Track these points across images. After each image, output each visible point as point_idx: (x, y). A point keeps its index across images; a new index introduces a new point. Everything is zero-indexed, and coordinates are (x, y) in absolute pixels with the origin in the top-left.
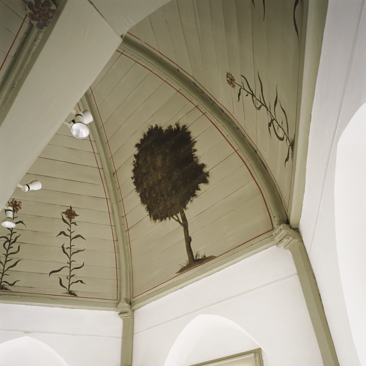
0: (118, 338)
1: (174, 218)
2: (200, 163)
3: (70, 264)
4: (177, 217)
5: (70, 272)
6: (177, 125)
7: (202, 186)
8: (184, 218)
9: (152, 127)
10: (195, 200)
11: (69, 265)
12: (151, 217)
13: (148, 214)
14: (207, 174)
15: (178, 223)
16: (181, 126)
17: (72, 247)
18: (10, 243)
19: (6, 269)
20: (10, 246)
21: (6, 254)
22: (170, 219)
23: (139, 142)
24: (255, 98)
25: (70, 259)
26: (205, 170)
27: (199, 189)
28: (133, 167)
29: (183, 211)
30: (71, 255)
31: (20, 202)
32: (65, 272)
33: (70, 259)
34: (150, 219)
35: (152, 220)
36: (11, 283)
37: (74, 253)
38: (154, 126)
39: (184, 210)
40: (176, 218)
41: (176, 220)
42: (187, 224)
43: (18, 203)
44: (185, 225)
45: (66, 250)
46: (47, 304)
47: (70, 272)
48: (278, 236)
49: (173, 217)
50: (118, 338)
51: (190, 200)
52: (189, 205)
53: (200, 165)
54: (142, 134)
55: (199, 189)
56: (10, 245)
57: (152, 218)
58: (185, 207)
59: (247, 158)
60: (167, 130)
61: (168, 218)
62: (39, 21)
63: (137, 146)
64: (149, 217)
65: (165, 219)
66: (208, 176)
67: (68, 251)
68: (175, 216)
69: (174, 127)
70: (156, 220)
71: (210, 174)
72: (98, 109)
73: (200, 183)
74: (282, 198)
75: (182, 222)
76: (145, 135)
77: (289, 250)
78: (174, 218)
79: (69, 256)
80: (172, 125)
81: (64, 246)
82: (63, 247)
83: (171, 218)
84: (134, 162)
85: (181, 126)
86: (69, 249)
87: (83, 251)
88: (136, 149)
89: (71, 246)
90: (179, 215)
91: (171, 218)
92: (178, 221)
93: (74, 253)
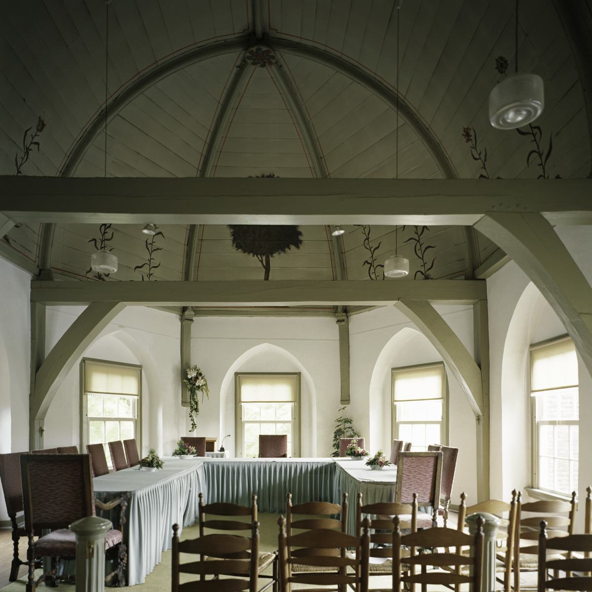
1: (258, 258)
2: (299, 230)
4: (262, 259)
5: (150, 269)
7: (292, 247)
8: (268, 262)
10: (282, 254)
11: (148, 262)
12: (233, 243)
13: (232, 238)
14: (301, 242)
15: (261, 263)
18: (105, 227)
20: (106, 231)
22: (254, 256)
24: (203, 501)
26: (301, 238)
27: (290, 249)
30: (152, 252)
32: (146, 269)
35: (235, 246)
37: (154, 250)
39: (270, 257)
40: (260, 259)
41: (260, 260)
42: (269, 269)
46: (359, 312)
47: (150, 269)
48: (23, 498)
52: (276, 255)
55: (290, 249)
57: (235, 245)
58: (272, 254)
61: (251, 254)
64: (231, 242)
65: (249, 253)
66: (301, 243)
67: (149, 247)
68: (259, 256)
70: (239, 248)
71: (303, 243)
72: (237, 108)
73: (292, 244)
74: (345, 264)
75: (265, 264)
77: (27, 277)
78: (258, 258)
81: (148, 241)
82: (146, 242)
83: (255, 256)
86: (151, 245)
87: (160, 249)
90: (264, 258)
91: (255, 256)
92: (262, 261)
93: (154, 250)
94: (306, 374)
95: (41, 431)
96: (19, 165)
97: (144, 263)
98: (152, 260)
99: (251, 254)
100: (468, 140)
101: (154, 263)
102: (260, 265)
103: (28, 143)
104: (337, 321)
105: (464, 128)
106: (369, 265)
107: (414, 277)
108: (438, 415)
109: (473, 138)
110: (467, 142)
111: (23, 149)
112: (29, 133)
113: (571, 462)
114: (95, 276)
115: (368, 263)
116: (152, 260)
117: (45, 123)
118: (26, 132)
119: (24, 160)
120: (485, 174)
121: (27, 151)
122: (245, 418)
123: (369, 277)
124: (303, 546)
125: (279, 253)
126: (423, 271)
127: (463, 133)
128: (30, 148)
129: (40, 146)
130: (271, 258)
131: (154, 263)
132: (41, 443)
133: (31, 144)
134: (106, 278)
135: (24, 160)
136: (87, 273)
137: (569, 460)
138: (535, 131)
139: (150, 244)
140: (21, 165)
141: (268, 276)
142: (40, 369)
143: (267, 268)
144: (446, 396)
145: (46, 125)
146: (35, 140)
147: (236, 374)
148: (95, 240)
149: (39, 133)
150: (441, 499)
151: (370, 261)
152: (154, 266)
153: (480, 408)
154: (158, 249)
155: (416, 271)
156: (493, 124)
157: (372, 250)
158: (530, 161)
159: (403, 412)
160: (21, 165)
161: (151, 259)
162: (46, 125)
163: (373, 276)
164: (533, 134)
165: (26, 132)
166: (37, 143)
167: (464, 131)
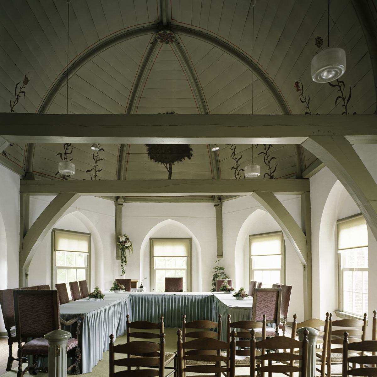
0: (362, 270)
3: (96, 167)
8: (171, 168)
11: (95, 168)
12: (149, 156)
13: (148, 153)
14: (191, 155)
17: (98, 156)
21: (65, 153)
22: (162, 164)
25: (96, 163)
26: (191, 152)
27: (184, 159)
29: (171, 165)
30: (97, 162)
32: (93, 172)
33: (96, 163)
34: (148, 156)
37: (98, 160)
39: (172, 164)
45: (95, 157)
49: (164, 164)
50: (362, 270)
51: (177, 161)
52: (175, 163)
53: (190, 148)
55: (184, 159)
56: (67, 147)
57: (149, 157)
59: (157, 45)
61: (160, 163)
62: (167, 34)
64: (147, 155)
65: (158, 162)
66: (192, 156)
67: (95, 158)
68: (165, 164)
70: (152, 159)
75: (169, 169)
77: (18, 177)
78: (164, 165)
83: (163, 164)
89: (97, 155)
90: (168, 165)
91: (163, 164)
92: (167, 167)
93: (98, 160)
94: (195, 240)
99: (160, 163)
100: (298, 90)
101: (99, 168)
103: (18, 92)
108: (279, 265)
109: (301, 88)
114: (61, 177)
115: (234, 168)
116: (97, 167)
117: (29, 79)
119: (16, 102)
121: (18, 97)
126: (269, 173)
129: (26, 94)
130: (172, 165)
131: (99, 168)
133: (20, 92)
135: (16, 102)
136: (56, 174)
138: (341, 84)
139: (96, 156)
140: (13, 106)
141: (171, 176)
143: (170, 172)
146: (22, 90)
148: (60, 154)
149: (25, 86)
154: (101, 159)
157: (237, 160)
158: (337, 104)
159: (257, 263)
160: (13, 106)
161: (96, 166)
163: (237, 177)
164: (339, 86)
166: (24, 92)
167: (295, 84)
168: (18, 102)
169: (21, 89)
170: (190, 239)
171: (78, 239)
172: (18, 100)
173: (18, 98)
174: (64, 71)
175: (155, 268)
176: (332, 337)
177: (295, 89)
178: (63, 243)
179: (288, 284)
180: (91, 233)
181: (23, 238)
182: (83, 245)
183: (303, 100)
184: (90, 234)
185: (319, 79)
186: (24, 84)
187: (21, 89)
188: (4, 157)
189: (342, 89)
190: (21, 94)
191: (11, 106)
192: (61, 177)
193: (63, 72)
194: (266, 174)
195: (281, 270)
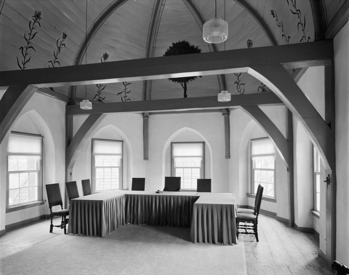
1: (181, 84)
3: (125, 90)
4: (182, 84)
5: (125, 94)
6: (197, 47)
8: (185, 85)
9: (185, 41)
11: (124, 91)
16: (199, 48)
19: (100, 90)
22: (178, 83)
23: (175, 43)
28: (166, 51)
29: (186, 83)
30: (32, 29)
31: (108, 55)
32: (123, 94)
36: (103, 98)
37: (127, 84)
38: (186, 41)
43: (107, 55)
44: (185, 88)
47: (125, 94)
49: (180, 82)
54: (179, 41)
55: (170, 47)
60: (191, 46)
61: (177, 82)
63: (173, 44)
65: (176, 81)
68: (181, 83)
69: (195, 47)
75: (184, 86)
76: (180, 42)
77: (64, 104)
78: (181, 84)
79: (31, 29)
80: (195, 46)
84: (168, 49)
85: (199, 48)
88: (172, 45)
90: (183, 83)
92: (182, 85)
93: (127, 84)
94: (207, 143)
95: (71, 174)
96: (56, 56)
97: (122, 91)
98: (126, 90)
99: (177, 82)
100: (274, 17)
101: (127, 91)
102: (182, 87)
103: (59, 45)
104: (223, 114)
105: (271, 10)
106: (237, 84)
107: (258, 90)
108: (199, 164)
109: (275, 15)
110: (274, 17)
111: (57, 48)
112: (59, 41)
113: (184, 177)
114: (97, 100)
115: (237, 83)
117: (67, 34)
118: (58, 41)
119: (58, 53)
120: (284, 34)
121: (59, 48)
122: (97, 164)
123: (237, 91)
124: (73, 200)
125: (191, 80)
126: (262, 87)
127: (271, 13)
128: (61, 47)
129: (65, 45)
130: (187, 83)
131: (127, 91)
132: (71, 178)
133: (61, 45)
134: (103, 100)
135: (58, 53)
136: (93, 99)
137: (184, 178)
138: (298, 12)
140: (57, 55)
141: (186, 92)
142: (70, 144)
143: (185, 88)
144: (43, 154)
145: (67, 36)
146: (63, 43)
147: (172, 143)
149: (64, 40)
150: (133, 189)
151: (237, 82)
152: (127, 92)
153: (287, 162)
155: (258, 88)
156: (204, 39)
157: (238, 75)
158: (299, 28)
159: (178, 162)
160: (57, 55)
161: (126, 89)
162: (67, 36)
163: (239, 90)
164: (297, 13)
165: (58, 41)
166: (64, 44)
167: (271, 12)
168: (60, 52)
169: (61, 43)
170: (204, 143)
171: (286, 125)
172: (60, 51)
173: (60, 49)
174: (94, 23)
175: (96, 165)
176: (85, 194)
177: (272, 16)
178: (99, 148)
179: (207, 177)
180: (124, 140)
181: (68, 146)
182: (116, 148)
183: (279, 25)
184: (122, 141)
185: (208, 39)
186: (63, 38)
187: (61, 43)
188: (52, 92)
189: (300, 17)
190: (62, 46)
191: (55, 56)
192: (97, 100)
193: (93, 24)
194: (260, 88)
195: (201, 169)
